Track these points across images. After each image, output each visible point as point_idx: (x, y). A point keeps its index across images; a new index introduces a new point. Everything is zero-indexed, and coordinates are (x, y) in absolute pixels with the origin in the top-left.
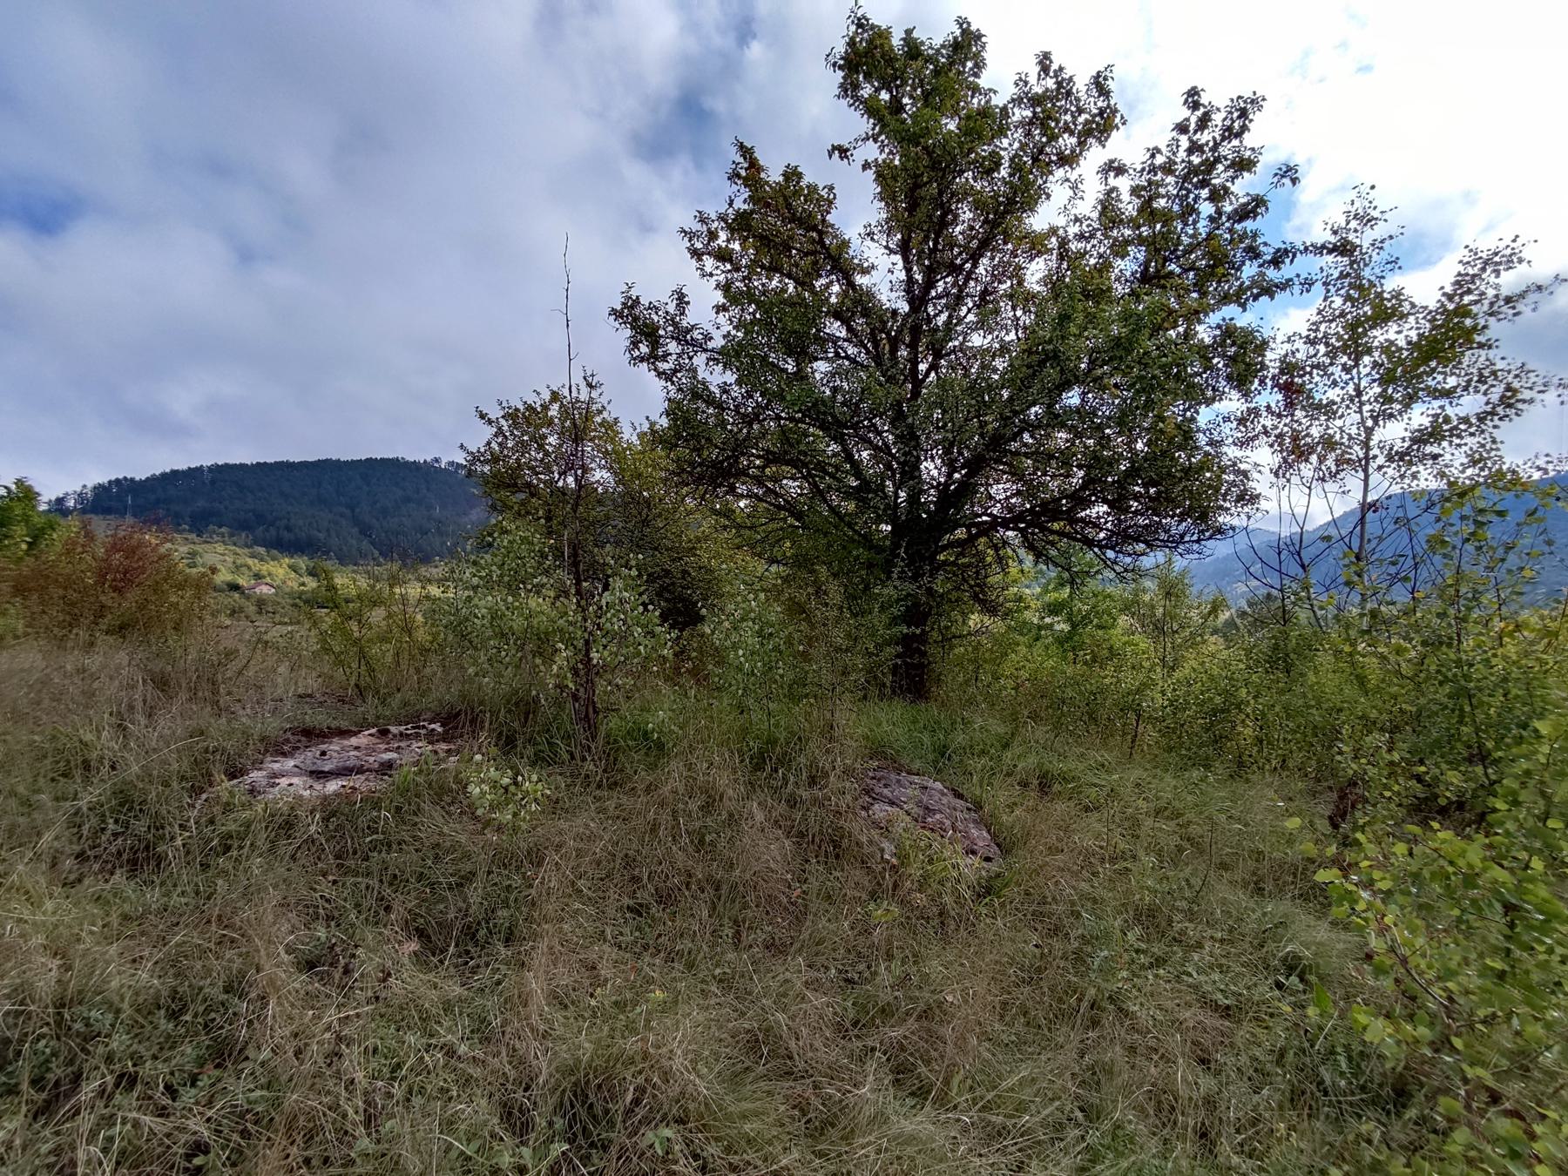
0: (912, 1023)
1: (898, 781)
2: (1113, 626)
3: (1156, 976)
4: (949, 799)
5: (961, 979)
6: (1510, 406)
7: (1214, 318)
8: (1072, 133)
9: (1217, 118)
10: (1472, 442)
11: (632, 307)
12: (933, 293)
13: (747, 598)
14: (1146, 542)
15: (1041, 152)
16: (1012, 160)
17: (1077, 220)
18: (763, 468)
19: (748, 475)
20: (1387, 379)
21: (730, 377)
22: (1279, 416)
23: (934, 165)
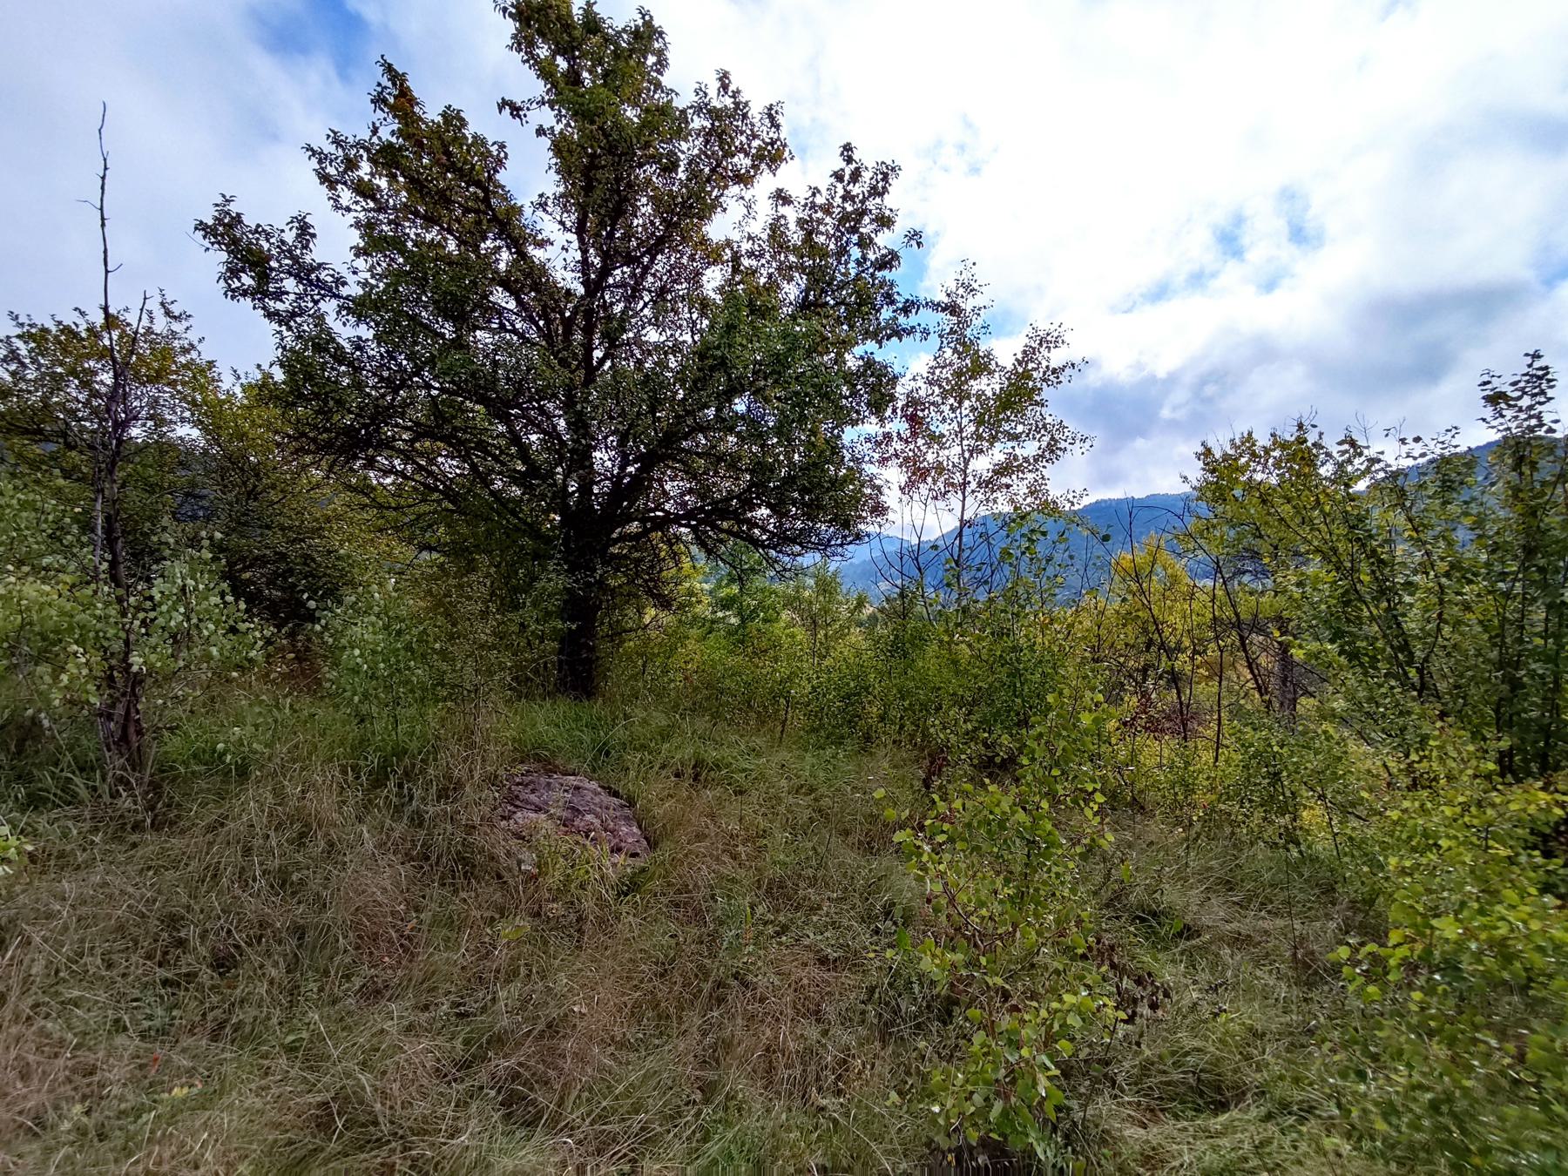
0: (529, 1047)
1: (549, 784)
2: (777, 620)
3: (780, 944)
4: (606, 799)
5: (587, 992)
6: (1052, 452)
7: (858, 350)
8: (747, 155)
9: (866, 176)
10: (1030, 476)
11: (230, 226)
12: (611, 281)
13: (385, 588)
14: (800, 544)
15: (718, 165)
16: (690, 163)
17: (750, 238)
18: (412, 441)
19: (393, 448)
20: (979, 422)
21: (366, 332)
22: (907, 442)
23: (611, 149)
